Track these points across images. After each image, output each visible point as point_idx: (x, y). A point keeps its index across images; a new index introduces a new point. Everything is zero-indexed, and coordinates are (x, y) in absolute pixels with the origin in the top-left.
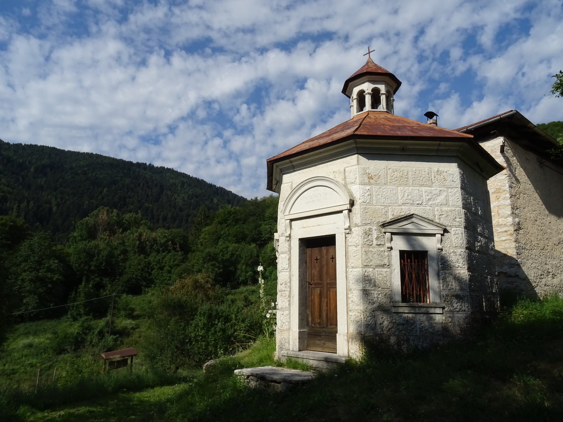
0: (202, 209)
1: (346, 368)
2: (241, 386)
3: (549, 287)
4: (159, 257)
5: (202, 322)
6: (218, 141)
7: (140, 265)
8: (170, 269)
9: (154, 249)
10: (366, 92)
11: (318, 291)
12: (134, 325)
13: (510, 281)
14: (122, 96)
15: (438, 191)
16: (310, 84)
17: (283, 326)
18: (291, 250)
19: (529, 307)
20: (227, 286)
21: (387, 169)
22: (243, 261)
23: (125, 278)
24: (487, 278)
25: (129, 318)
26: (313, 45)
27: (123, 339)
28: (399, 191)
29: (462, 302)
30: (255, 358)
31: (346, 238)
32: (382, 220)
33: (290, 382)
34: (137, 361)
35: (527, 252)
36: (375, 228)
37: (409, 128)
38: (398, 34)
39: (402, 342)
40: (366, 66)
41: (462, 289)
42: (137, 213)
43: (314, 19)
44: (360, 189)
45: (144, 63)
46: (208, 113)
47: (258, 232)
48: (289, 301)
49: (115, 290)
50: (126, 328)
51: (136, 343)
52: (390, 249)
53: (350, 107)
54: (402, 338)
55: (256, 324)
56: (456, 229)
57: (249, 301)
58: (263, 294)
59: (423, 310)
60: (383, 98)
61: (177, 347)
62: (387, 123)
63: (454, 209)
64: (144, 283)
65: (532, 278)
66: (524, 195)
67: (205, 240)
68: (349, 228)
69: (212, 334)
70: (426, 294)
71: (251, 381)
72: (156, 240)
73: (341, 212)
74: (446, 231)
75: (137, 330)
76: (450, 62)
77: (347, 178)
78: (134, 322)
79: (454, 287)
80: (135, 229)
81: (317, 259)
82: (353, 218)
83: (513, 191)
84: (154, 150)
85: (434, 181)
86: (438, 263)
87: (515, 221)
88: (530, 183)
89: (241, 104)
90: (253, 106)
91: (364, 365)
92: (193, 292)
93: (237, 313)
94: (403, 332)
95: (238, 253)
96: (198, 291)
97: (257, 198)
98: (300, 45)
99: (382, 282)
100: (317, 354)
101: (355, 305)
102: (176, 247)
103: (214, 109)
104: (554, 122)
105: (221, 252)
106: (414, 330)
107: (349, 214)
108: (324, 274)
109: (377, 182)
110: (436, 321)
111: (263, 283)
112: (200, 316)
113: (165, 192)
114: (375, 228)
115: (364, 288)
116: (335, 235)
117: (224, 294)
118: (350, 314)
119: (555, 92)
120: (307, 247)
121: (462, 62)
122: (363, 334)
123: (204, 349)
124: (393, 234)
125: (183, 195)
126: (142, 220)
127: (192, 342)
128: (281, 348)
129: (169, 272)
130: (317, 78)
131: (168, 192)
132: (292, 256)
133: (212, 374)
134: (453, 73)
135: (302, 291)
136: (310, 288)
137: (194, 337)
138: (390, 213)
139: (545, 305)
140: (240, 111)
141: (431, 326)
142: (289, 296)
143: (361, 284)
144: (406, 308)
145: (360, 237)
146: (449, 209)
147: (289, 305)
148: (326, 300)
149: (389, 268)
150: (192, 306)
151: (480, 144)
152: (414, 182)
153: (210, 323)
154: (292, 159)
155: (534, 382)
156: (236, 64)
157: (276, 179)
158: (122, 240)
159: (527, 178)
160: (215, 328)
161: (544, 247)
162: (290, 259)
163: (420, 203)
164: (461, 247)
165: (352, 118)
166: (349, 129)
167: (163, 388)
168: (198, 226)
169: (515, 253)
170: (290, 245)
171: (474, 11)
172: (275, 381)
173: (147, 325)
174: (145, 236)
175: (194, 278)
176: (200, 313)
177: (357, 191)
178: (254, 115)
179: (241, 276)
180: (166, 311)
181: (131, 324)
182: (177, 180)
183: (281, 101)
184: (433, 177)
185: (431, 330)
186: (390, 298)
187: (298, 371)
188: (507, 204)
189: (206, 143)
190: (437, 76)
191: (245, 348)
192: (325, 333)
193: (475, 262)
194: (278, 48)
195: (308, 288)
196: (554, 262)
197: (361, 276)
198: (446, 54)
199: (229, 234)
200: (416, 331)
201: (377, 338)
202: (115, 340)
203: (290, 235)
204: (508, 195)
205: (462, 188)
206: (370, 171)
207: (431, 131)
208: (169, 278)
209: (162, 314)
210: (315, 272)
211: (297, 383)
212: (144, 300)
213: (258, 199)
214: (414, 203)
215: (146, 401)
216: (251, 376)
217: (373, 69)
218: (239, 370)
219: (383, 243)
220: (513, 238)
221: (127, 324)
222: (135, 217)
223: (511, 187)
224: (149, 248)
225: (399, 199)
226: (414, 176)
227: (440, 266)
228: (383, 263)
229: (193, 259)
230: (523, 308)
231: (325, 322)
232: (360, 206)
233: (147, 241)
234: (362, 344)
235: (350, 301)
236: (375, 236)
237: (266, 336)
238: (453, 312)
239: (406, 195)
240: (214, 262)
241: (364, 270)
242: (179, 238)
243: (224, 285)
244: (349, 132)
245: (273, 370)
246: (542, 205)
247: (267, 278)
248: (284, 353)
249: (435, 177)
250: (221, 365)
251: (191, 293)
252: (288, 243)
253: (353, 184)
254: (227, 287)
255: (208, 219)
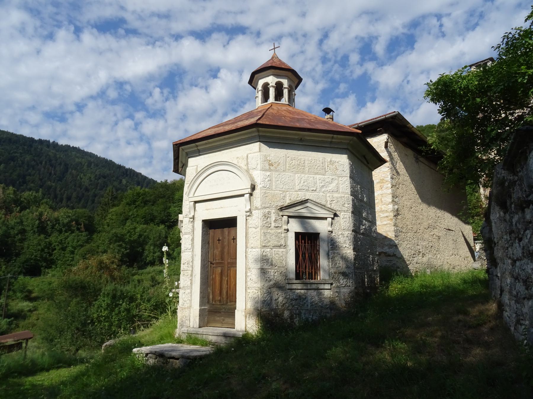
0: (109, 190)
1: (243, 342)
2: (139, 364)
3: (419, 265)
4: (62, 237)
5: (105, 302)
6: (128, 123)
7: (40, 245)
8: (73, 249)
9: (56, 229)
10: (271, 85)
11: (219, 270)
12: (31, 307)
13: (389, 260)
14: (23, 69)
15: (330, 179)
16: (223, 73)
17: (184, 304)
18: (194, 230)
19: (402, 282)
20: (134, 266)
21: (286, 157)
22: (151, 242)
23: (22, 258)
24: (369, 257)
25: (26, 300)
26: (227, 38)
27: (18, 322)
28: (296, 178)
29: (347, 279)
30: (156, 336)
31: (246, 220)
32: (280, 204)
33: (188, 358)
34: (34, 344)
35: (403, 235)
36: (273, 211)
37: (307, 121)
38: (305, 36)
39: (295, 316)
40: (271, 61)
41: (347, 267)
42: (37, 191)
43: (228, 12)
44: (260, 174)
45: (51, 37)
46: (119, 93)
47: (167, 213)
48: (191, 280)
49: (10, 271)
50: (22, 311)
51: (34, 325)
52: (286, 231)
53: (256, 98)
54: (295, 312)
55: (162, 304)
56: (344, 213)
57: (156, 281)
58: (167, 273)
59: (314, 286)
60: (286, 92)
61: (78, 329)
62: (288, 115)
63: (343, 195)
64: (44, 264)
65: (406, 257)
66: (403, 186)
67: (111, 221)
68: (250, 211)
69: (116, 314)
70: (317, 272)
71: (149, 358)
72: (59, 220)
73: (242, 195)
74: (336, 215)
75: (34, 312)
76: (349, 66)
77: (249, 163)
78: (31, 304)
79: (341, 265)
80: (34, 208)
81: (219, 240)
82: (253, 202)
83: (394, 182)
84: (60, 127)
85: (327, 170)
86: (328, 244)
87: (394, 208)
88: (408, 175)
89: (154, 88)
90: (166, 91)
91: (260, 338)
92: (97, 273)
93: (142, 293)
94: (296, 306)
95: (145, 234)
96: (103, 272)
97: (167, 180)
98: (215, 36)
99: (278, 261)
100: (217, 329)
101: (253, 282)
102: (81, 227)
103: (126, 90)
104: (430, 125)
105: (129, 232)
106: (306, 304)
107: (250, 198)
108: (225, 254)
109: (277, 169)
110: (325, 296)
111: (167, 263)
112: (104, 297)
113: (70, 170)
114: (273, 211)
115: (262, 267)
116: (237, 217)
117: (130, 274)
118: (248, 291)
119: (426, 98)
120: (210, 229)
121: (359, 66)
122: (259, 309)
123: (108, 329)
124: (289, 217)
125: (90, 175)
126: (43, 198)
127: (94, 323)
128: (182, 326)
129: (72, 252)
130: (230, 68)
131: (73, 171)
132: (195, 236)
133: (110, 354)
134: (351, 76)
135: (204, 270)
136: (212, 268)
137: (97, 318)
138: (287, 198)
139: (415, 280)
140: (153, 94)
141: (321, 300)
142: (191, 275)
143: (259, 263)
144: (299, 284)
145: (260, 220)
146: (339, 195)
147: (191, 283)
148: (226, 279)
149: (285, 248)
150: (95, 287)
151: (368, 140)
152: (310, 170)
153: (114, 304)
154: (197, 144)
155: (401, 346)
156: (150, 47)
157: (182, 162)
158: (20, 219)
159: (405, 171)
160: (120, 308)
161: (417, 230)
162: (193, 240)
163: (315, 190)
164: (348, 230)
165: (257, 108)
166: (253, 118)
167: (59, 371)
168: (104, 207)
169: (394, 236)
170: (193, 227)
171: (370, 22)
172: (173, 358)
173: (46, 307)
174: (46, 215)
175: (99, 259)
176: (104, 294)
177: (258, 177)
178: (167, 99)
179: (148, 257)
180: (66, 292)
181: (28, 306)
182: (83, 160)
183: (194, 88)
184: (326, 167)
185: (320, 304)
186: (285, 276)
187: (197, 346)
188: (388, 193)
189: (116, 124)
190: (337, 77)
191: (146, 326)
192: (225, 310)
193: (359, 243)
194: (193, 36)
195: (209, 267)
196: (424, 244)
197: (260, 255)
198: (346, 58)
199: (138, 215)
200: (308, 305)
201: (273, 313)
202: (10, 324)
203: (194, 216)
204: (390, 185)
205: (350, 177)
206: (271, 158)
207: (326, 125)
208: (71, 259)
209: (62, 295)
210: (217, 252)
211: (195, 358)
212: (43, 282)
213: (168, 181)
214: (310, 189)
215: (39, 384)
216: (150, 354)
217: (277, 64)
218: (138, 349)
219: (280, 225)
220: (392, 223)
221: (24, 306)
222: (35, 195)
223: (392, 178)
224: (50, 228)
225: (296, 185)
226: (310, 165)
227: (330, 247)
228: (280, 244)
229: (98, 240)
230: (398, 283)
231: (225, 299)
232: (261, 190)
233: (49, 220)
234: (258, 319)
235: (248, 279)
236: (273, 218)
237: (168, 314)
238: (340, 287)
239: (302, 182)
240: (121, 243)
241: (262, 250)
242: (84, 218)
243: (130, 265)
244: (253, 120)
245: (173, 347)
246: (416, 195)
247: (175, 259)
248: (184, 330)
249: (328, 166)
250: (121, 344)
251: (96, 274)
252: (192, 224)
253: (255, 170)
254: (134, 268)
255: (115, 200)
